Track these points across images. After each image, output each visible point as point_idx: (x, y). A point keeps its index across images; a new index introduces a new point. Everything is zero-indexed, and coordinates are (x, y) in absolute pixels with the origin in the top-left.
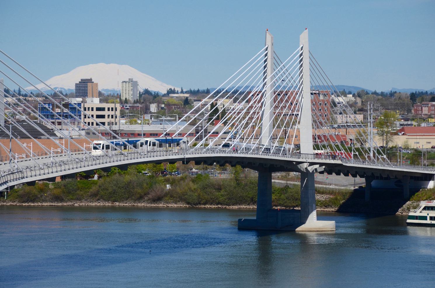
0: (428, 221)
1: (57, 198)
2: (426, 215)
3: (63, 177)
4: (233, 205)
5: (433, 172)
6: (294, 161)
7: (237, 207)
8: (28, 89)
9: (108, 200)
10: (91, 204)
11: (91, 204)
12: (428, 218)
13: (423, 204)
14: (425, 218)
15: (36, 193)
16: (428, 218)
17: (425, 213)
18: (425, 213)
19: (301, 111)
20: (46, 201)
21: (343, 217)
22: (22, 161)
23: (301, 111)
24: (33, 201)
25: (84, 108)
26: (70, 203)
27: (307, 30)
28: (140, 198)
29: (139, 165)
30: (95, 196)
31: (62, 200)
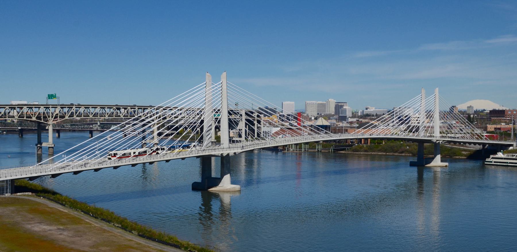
0: (493, 163)
1: (366, 151)
2: (492, 161)
3: (323, 141)
4: (430, 155)
5: (266, 146)
6: (321, 141)
7: (431, 156)
8: (462, 107)
9: (384, 152)
10: (378, 153)
11: (378, 153)
12: (493, 162)
13: (491, 156)
14: (492, 162)
15: (359, 149)
16: (493, 162)
17: (492, 160)
18: (492, 160)
19: (342, 103)
20: (362, 152)
21: (474, 162)
22: (146, 219)
23: (342, 103)
24: (358, 152)
25: (253, 112)
26: (371, 153)
27: (226, 72)
28: (396, 152)
29: (18, 180)
30: (380, 151)
31: (368, 152)
